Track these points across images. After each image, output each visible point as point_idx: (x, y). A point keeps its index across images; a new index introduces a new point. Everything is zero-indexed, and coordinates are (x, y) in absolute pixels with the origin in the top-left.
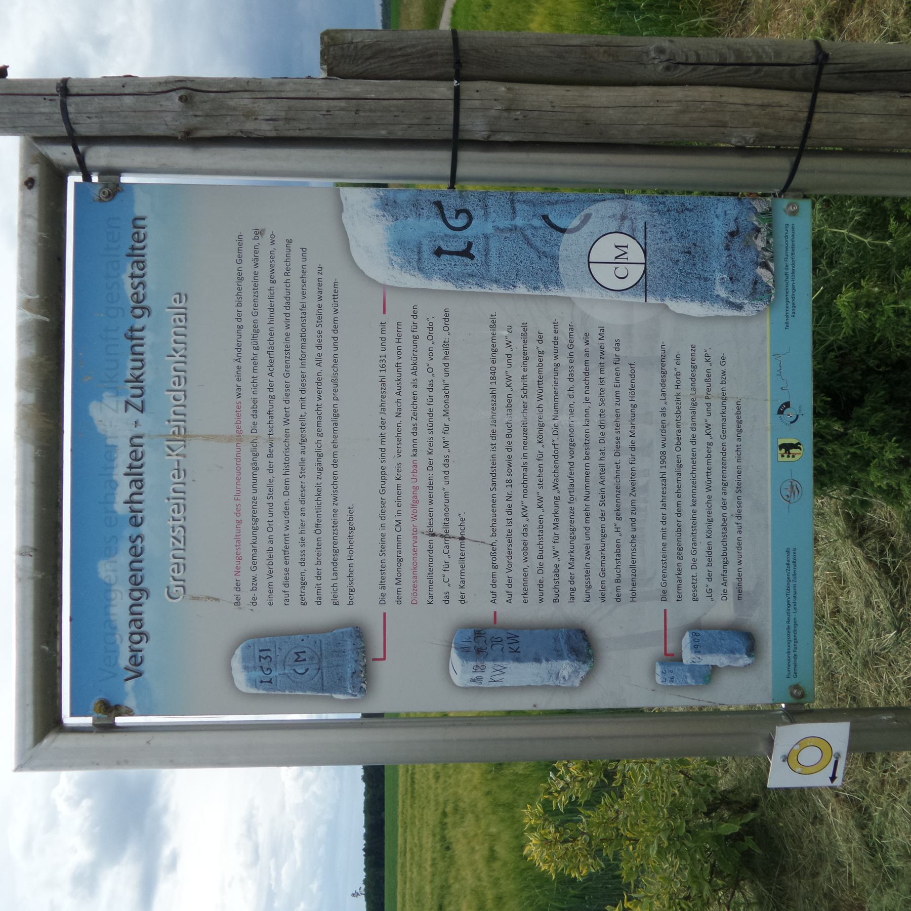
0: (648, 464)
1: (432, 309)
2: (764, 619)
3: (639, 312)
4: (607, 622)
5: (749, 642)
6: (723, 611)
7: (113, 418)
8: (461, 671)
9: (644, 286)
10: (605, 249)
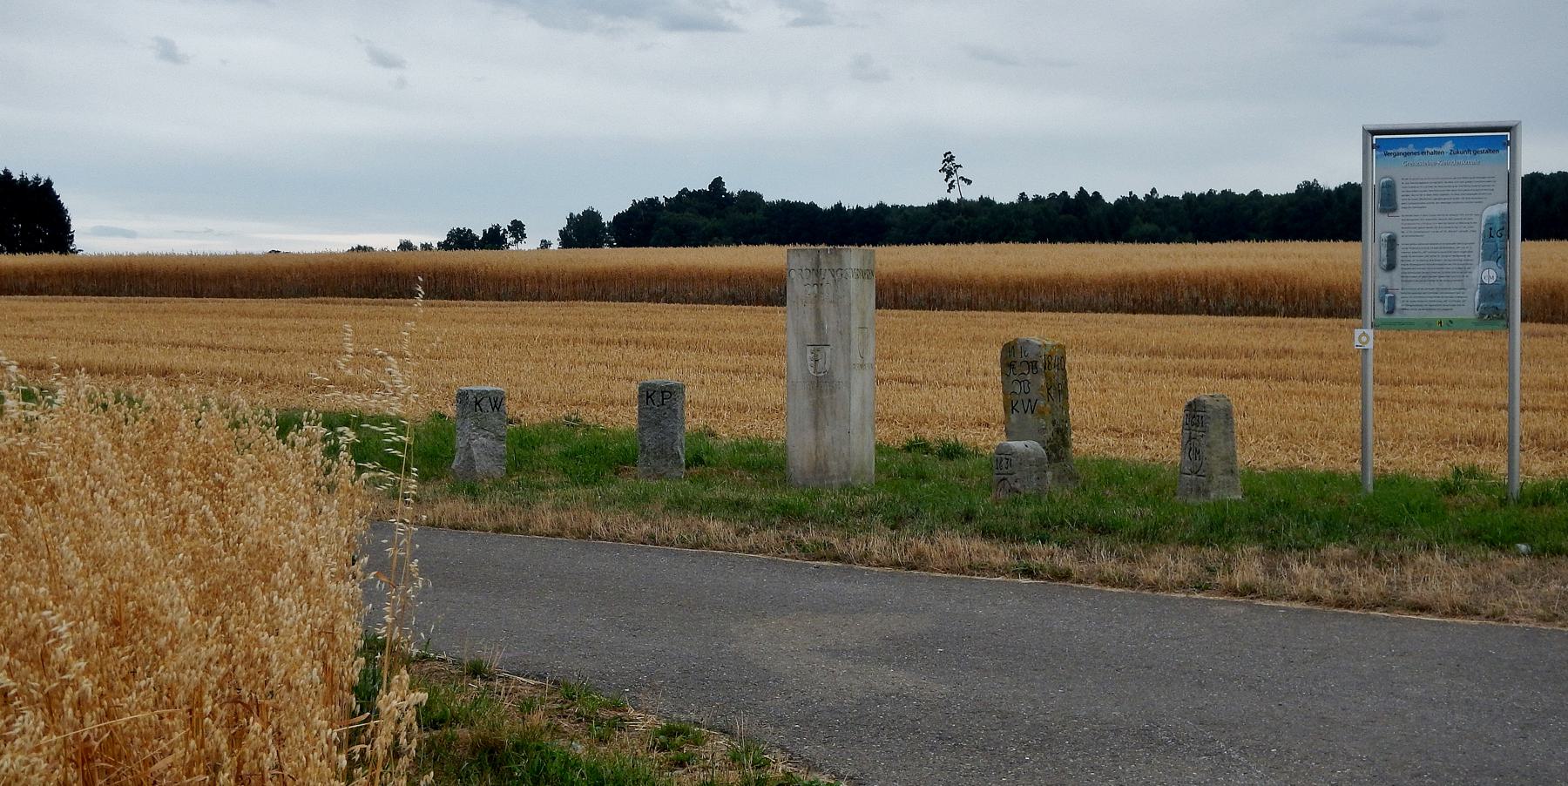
0: (1436, 285)
1: (1476, 227)
2: (1397, 316)
3: (1476, 283)
4: (1396, 274)
5: (1391, 311)
6: (1399, 305)
7: (1448, 146)
8: (1385, 236)
9: (1483, 284)
10: (1492, 273)
